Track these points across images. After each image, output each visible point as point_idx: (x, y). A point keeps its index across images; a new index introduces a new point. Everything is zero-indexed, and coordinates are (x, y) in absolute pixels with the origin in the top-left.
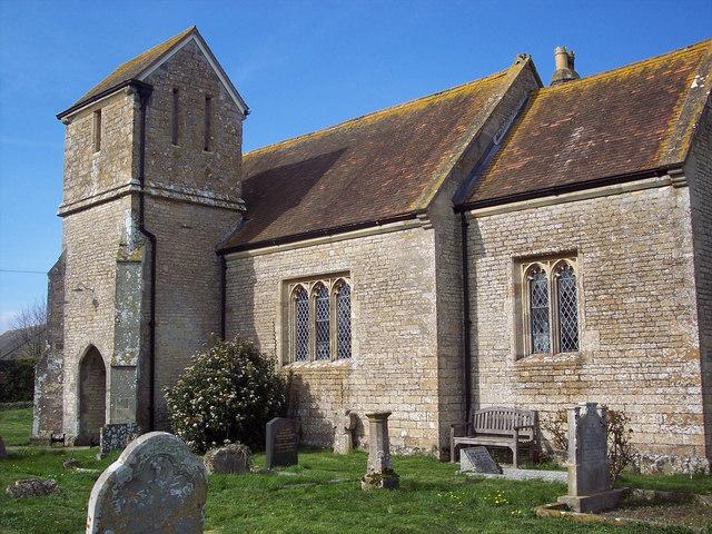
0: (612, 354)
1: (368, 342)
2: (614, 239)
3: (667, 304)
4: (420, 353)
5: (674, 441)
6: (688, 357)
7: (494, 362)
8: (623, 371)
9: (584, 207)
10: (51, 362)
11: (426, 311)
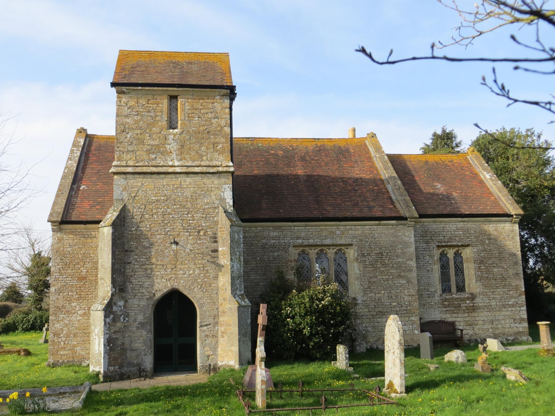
0: (488, 293)
1: (369, 287)
2: (487, 242)
3: (511, 272)
4: (407, 294)
5: (516, 330)
6: (520, 295)
7: (428, 297)
8: (493, 301)
9: (473, 226)
10: (115, 304)
11: (410, 270)
